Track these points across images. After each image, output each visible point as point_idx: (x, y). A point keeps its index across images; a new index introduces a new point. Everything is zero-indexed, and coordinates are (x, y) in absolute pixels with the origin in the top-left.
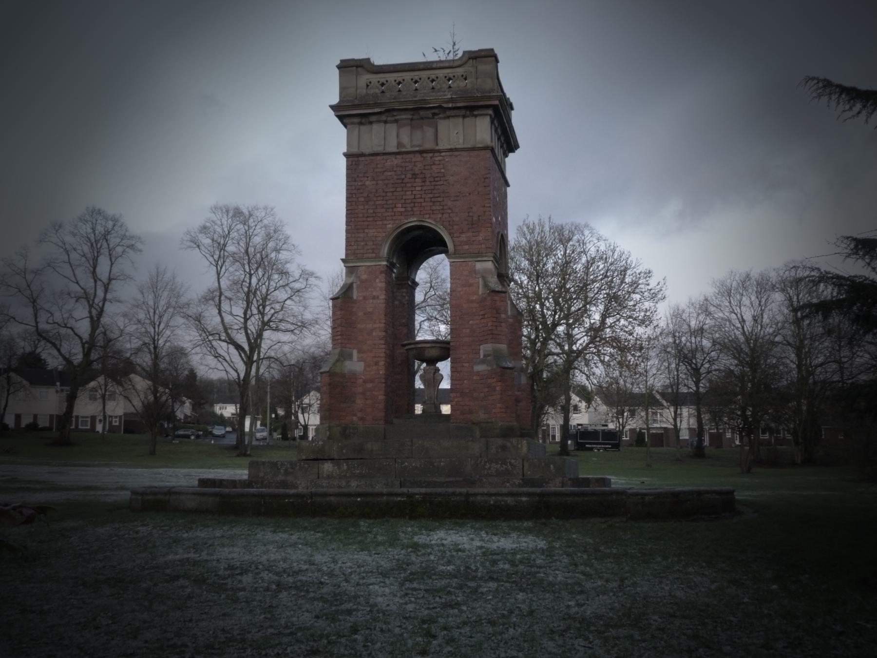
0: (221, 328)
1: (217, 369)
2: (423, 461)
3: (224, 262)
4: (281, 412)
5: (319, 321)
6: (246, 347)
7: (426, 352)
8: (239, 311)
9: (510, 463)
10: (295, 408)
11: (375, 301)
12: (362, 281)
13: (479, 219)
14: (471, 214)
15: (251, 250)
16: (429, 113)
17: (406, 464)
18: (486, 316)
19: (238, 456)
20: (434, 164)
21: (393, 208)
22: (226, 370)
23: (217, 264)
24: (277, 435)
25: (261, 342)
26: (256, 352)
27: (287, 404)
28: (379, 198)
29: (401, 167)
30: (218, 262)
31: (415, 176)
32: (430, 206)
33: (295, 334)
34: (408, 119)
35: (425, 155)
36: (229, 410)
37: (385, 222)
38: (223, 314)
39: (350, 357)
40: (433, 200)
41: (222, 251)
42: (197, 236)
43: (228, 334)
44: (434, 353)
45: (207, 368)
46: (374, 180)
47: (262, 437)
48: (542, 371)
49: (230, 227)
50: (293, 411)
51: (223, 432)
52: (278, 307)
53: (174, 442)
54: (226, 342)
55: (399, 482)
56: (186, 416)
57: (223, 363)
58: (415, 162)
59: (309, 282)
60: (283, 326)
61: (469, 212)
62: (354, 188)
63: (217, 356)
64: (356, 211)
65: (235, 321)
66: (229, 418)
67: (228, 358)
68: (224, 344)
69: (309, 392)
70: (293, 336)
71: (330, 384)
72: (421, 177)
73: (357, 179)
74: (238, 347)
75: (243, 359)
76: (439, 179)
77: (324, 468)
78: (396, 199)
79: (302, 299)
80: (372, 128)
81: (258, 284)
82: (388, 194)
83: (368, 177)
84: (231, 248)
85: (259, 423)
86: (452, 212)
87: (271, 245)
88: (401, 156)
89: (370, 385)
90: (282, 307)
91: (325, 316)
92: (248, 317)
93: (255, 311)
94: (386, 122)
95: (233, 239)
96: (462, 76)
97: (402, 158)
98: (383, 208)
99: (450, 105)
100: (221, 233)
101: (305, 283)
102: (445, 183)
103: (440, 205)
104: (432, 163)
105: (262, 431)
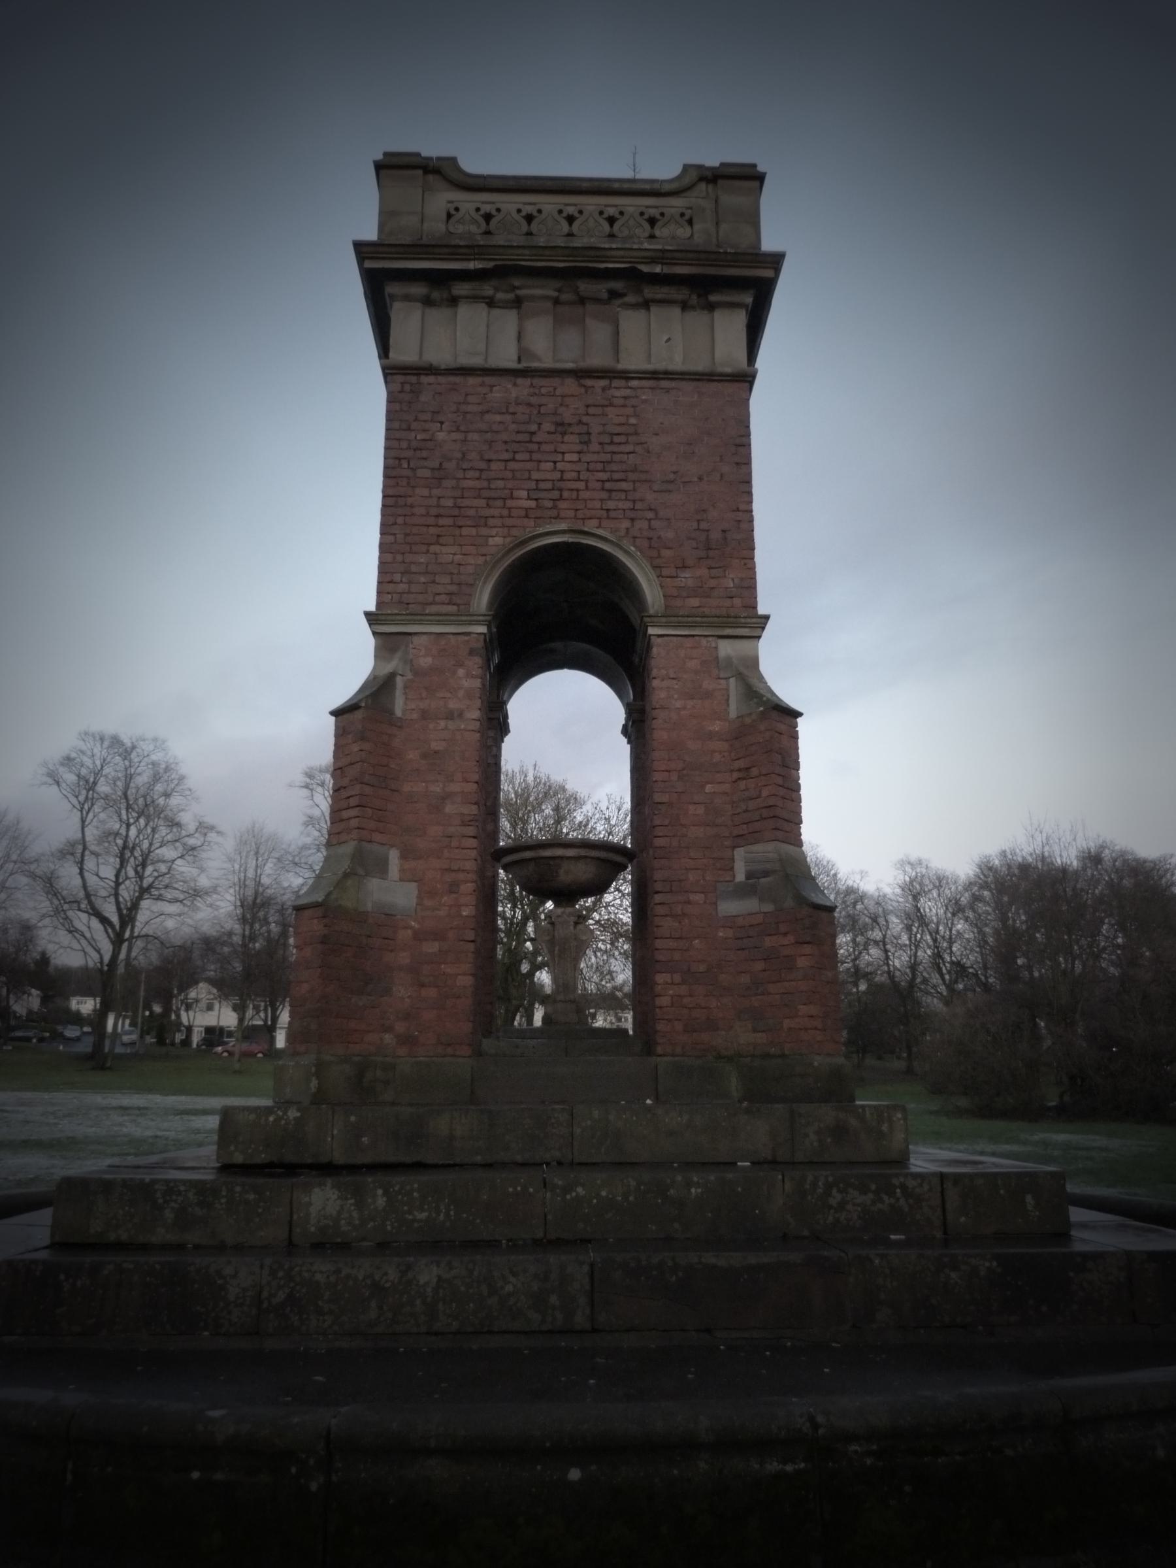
0: (82, 894)
1: (72, 948)
2: (633, 1183)
3: (93, 805)
4: (157, 1009)
5: (219, 889)
6: (115, 919)
7: (562, 871)
8: (108, 872)
9: (903, 1187)
10: (177, 1003)
11: (451, 725)
12: (418, 673)
13: (725, 539)
14: (703, 525)
15: (131, 792)
16: (601, 288)
17: (580, 1190)
18: (754, 771)
19: (93, 1069)
20: (611, 405)
21: (504, 499)
22: (84, 951)
23: (82, 808)
24: (150, 1039)
25: (136, 914)
26: (130, 927)
27: (166, 999)
28: (470, 474)
29: (529, 405)
30: (83, 804)
31: (562, 427)
32: (602, 500)
33: (184, 905)
34: (547, 298)
35: (589, 382)
36: (86, 1006)
37: (484, 531)
38: (86, 874)
39: (382, 869)
40: (608, 485)
41: (91, 792)
42: (57, 769)
43: (90, 903)
44: (582, 872)
45: (57, 946)
46: (458, 430)
47: (129, 1041)
48: (520, 962)
49: (104, 760)
50: (174, 1008)
51: (78, 1033)
52: (163, 868)
53: (5, 1048)
54: (86, 912)
55: (586, 1268)
56: (30, 1012)
57: (81, 941)
58: (563, 396)
59: (208, 839)
60: (168, 895)
61: (698, 521)
62: (404, 445)
63: (72, 931)
64: (410, 501)
65: (102, 884)
66: (89, 1015)
67: (88, 935)
68: (84, 916)
69: (197, 983)
70: (181, 907)
71: (324, 940)
72: (577, 431)
73: (414, 425)
74: (104, 921)
75: (109, 936)
76: (622, 439)
77: (310, 1204)
78: (514, 478)
79: (197, 859)
80: (456, 313)
81: (138, 836)
82: (494, 466)
83: (442, 423)
84: (103, 788)
85: (127, 1022)
86: (657, 518)
87: (159, 788)
88: (528, 381)
89: (432, 947)
90: (170, 869)
91: (227, 882)
92: (121, 880)
93: (131, 873)
94: (491, 303)
95: (106, 776)
96: (682, 215)
97: (532, 385)
98: (479, 497)
99: (658, 269)
100: (91, 767)
101: (202, 839)
102: (639, 449)
103: (626, 499)
104: (606, 403)
105: (130, 1033)
